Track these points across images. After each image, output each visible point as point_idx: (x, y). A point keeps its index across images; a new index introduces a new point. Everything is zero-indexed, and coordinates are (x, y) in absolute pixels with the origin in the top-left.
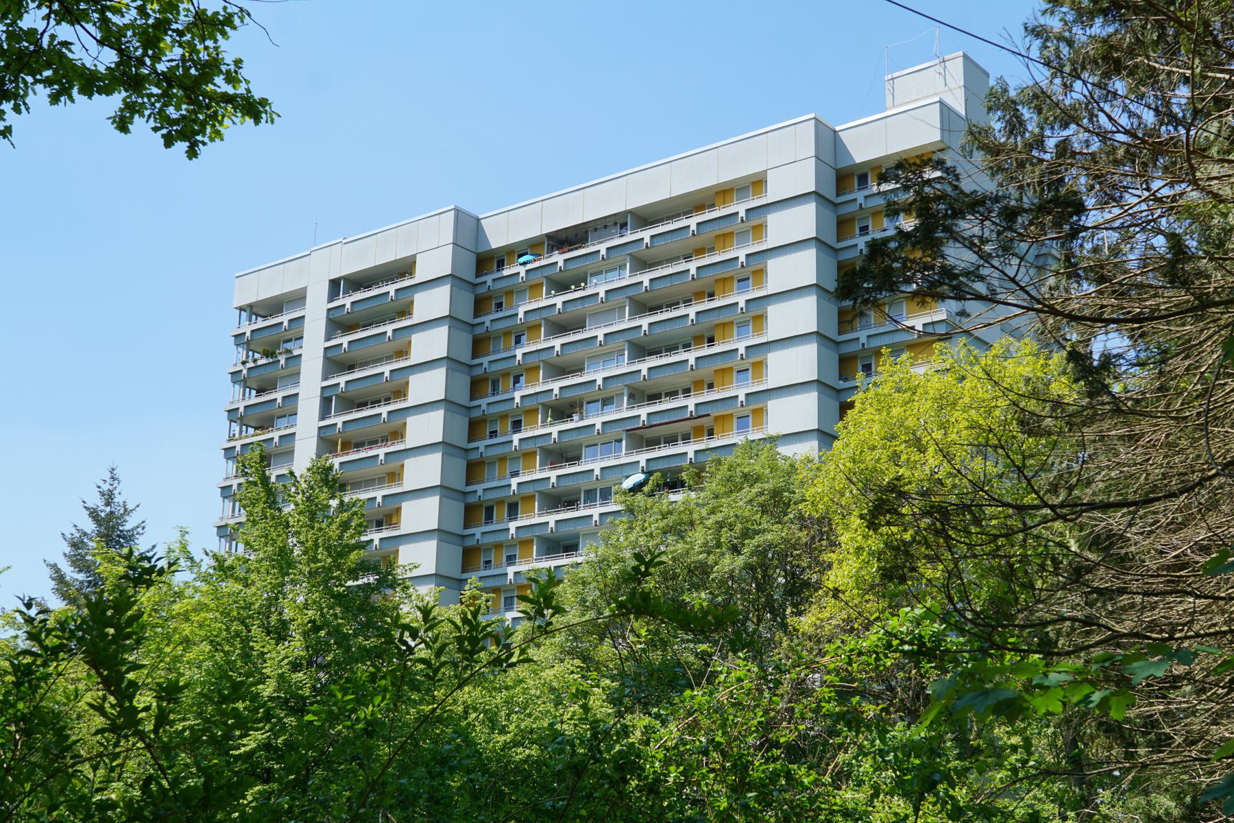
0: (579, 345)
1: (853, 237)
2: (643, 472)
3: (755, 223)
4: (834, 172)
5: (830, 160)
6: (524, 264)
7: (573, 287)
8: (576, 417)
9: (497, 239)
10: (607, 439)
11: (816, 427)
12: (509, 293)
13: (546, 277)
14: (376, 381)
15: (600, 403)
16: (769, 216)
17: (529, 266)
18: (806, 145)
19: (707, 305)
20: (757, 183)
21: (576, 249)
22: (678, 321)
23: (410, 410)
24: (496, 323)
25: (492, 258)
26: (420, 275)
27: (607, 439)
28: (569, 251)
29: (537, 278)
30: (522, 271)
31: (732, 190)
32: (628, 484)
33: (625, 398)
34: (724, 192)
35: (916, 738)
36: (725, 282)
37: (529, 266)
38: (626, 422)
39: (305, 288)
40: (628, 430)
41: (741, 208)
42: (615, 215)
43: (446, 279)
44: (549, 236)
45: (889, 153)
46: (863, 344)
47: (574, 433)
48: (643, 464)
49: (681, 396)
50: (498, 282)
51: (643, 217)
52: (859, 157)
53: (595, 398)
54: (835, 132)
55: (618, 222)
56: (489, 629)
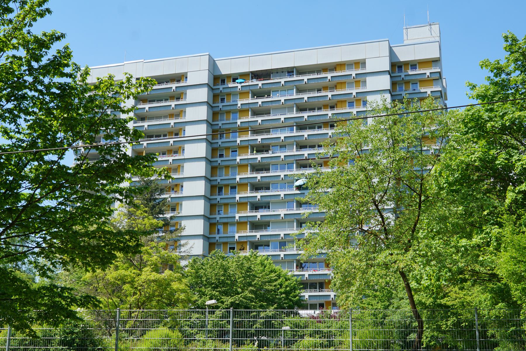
0: (270, 121)
1: (218, 103)
3: (360, 80)
4: (213, 76)
5: (212, 72)
6: (241, 83)
7: (266, 96)
8: (270, 152)
9: (225, 69)
11: (204, 175)
12: (229, 94)
13: (251, 90)
14: (166, 127)
15: (279, 147)
17: (243, 84)
18: (205, 65)
20: (361, 63)
21: (267, 80)
22: (322, 116)
23: (186, 142)
24: (225, 107)
25: (219, 78)
27: (286, 164)
28: (264, 80)
29: (246, 90)
30: (239, 86)
31: (345, 64)
33: (295, 146)
34: (341, 65)
35: (513, 292)
36: (343, 102)
37: (243, 84)
38: (296, 157)
39: (187, 73)
41: (353, 73)
42: (288, 68)
44: (252, 73)
45: (232, 72)
46: (220, 145)
49: (316, 148)
50: (225, 89)
51: (301, 71)
52: (224, 72)
54: (214, 60)
55: (290, 71)
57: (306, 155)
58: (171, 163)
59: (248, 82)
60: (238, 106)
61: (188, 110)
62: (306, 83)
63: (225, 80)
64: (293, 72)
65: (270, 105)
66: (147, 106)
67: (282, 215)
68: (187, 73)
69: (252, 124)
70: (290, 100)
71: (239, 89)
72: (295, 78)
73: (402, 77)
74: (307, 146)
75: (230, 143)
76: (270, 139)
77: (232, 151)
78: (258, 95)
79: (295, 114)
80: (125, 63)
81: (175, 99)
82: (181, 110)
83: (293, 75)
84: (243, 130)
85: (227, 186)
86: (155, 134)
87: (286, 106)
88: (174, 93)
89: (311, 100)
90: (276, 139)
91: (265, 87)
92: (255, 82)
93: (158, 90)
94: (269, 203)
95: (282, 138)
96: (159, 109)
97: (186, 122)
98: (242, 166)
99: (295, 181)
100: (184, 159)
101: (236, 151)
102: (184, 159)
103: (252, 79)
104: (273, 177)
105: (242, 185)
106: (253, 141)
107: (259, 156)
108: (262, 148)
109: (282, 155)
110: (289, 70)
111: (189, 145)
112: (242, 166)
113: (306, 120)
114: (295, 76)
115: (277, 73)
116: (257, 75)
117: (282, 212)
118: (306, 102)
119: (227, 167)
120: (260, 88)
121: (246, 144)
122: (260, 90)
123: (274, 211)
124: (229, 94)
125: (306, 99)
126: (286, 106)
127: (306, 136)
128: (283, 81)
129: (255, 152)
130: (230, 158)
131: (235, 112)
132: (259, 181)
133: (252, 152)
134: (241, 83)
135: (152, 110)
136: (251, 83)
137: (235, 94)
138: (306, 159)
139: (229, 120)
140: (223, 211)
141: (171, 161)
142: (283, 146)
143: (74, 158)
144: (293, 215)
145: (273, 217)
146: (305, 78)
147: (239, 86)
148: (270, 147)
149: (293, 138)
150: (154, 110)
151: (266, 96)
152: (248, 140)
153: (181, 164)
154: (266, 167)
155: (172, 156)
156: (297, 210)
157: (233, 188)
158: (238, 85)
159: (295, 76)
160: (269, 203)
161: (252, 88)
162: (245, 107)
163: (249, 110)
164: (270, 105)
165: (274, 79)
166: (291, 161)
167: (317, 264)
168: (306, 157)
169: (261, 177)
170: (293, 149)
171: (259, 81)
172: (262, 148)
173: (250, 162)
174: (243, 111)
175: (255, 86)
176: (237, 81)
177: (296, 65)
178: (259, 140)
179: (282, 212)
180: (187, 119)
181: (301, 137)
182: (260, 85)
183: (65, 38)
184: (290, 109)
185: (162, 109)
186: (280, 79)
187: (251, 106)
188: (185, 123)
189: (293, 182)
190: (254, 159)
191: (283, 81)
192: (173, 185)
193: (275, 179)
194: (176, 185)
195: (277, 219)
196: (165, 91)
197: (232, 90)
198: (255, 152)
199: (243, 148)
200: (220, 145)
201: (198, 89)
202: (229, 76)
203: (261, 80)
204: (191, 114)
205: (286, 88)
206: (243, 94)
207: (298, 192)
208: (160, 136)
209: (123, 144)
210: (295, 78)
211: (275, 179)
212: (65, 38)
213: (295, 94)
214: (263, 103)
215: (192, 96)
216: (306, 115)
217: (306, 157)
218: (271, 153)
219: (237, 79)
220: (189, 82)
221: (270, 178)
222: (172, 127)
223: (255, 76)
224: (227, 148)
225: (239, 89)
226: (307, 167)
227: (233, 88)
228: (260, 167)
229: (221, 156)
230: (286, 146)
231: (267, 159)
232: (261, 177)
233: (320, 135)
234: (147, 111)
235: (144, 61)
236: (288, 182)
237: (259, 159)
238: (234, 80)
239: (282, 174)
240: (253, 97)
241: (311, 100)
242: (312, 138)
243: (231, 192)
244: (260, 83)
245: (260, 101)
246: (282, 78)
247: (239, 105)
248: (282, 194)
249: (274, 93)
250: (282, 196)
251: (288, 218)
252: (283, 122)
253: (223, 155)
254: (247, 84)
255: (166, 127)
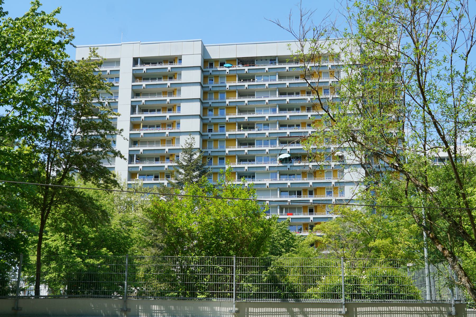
2: (288, 153)
6: (229, 67)
8: (256, 129)
10: (270, 140)
12: (217, 77)
14: (162, 103)
15: (263, 125)
16: (181, 104)
17: (231, 69)
19: (252, 115)
26: (184, 63)
27: (270, 140)
30: (228, 70)
32: (283, 156)
37: (231, 69)
39: (120, 58)
40: (279, 137)
43: (198, 67)
44: (239, 59)
45: (221, 57)
47: (255, 135)
48: (288, 150)
51: (282, 60)
53: (261, 123)
55: (272, 60)
56: (360, 107)
57: (288, 133)
58: (167, 135)
59: (235, 67)
60: (227, 87)
61: (183, 89)
62: (287, 71)
63: (213, 63)
64: (275, 60)
65: (255, 88)
66: (144, 84)
67: (268, 185)
68: (181, 56)
69: (239, 104)
70: (274, 85)
71: (228, 73)
72: (277, 66)
73: (210, 88)
74: (148, 110)
75: (220, 119)
76: (256, 118)
77: (220, 127)
78: (244, 79)
79: (277, 97)
80: (122, 43)
81: (168, 78)
82: (176, 88)
83: (276, 63)
84: (230, 108)
85: (216, 157)
86: (149, 109)
87: (270, 90)
88: (169, 73)
89: (292, 86)
90: (261, 118)
91: (251, 72)
92: (241, 67)
93: (154, 70)
94: (254, 173)
95: (267, 117)
96: (155, 87)
97: (181, 99)
98: (230, 141)
99: (278, 155)
100: (180, 132)
101: (224, 127)
102: (180, 132)
103: (238, 64)
104: (259, 151)
105: (231, 157)
106: (240, 119)
107: (246, 133)
108: (249, 126)
109: (267, 132)
110: (273, 59)
111: (184, 120)
112: (230, 141)
113: (288, 103)
114: (277, 64)
115: (262, 60)
116: (243, 61)
117: (267, 182)
118: (288, 87)
119: (216, 140)
120: (246, 72)
121: (234, 121)
122: (247, 74)
123: (260, 181)
124: (217, 77)
125: (288, 84)
126: (270, 90)
127: (288, 117)
128: (267, 68)
129: (242, 128)
130: (219, 133)
131: (222, 92)
132: (246, 154)
133: (239, 128)
134: (229, 67)
135: (148, 87)
136: (238, 68)
137: (222, 77)
138: (288, 137)
139: (217, 99)
140: (212, 179)
141: (167, 133)
142: (266, 125)
143: (84, 58)
144: (277, 185)
145: (259, 185)
146: (287, 66)
147: (228, 70)
148: (254, 124)
149: (276, 118)
150: (151, 87)
151: (252, 80)
152: (236, 118)
153: (177, 137)
154: (252, 142)
155: (168, 129)
156: (280, 180)
157: (222, 159)
158: (226, 69)
159: (277, 64)
160: (254, 173)
161: (238, 72)
162: (232, 89)
163: (236, 91)
164: (255, 88)
165: (259, 66)
166: (275, 137)
167: (297, 226)
168: (288, 135)
169: (248, 150)
170: (276, 127)
171: (246, 66)
172: (249, 126)
173: (238, 137)
174: (231, 92)
175: (242, 71)
176: (225, 65)
177: (278, 55)
178: (246, 118)
179: (267, 182)
180: (183, 96)
181: (283, 117)
182: (246, 70)
183: (60, 13)
184: (273, 92)
185: (158, 87)
186: (265, 65)
187: (238, 88)
188: (180, 101)
189: (276, 156)
190: (242, 135)
191: (267, 68)
192: (169, 155)
193: (259, 153)
194: (172, 155)
195: (263, 187)
196: (161, 71)
197: (221, 73)
198: (242, 128)
199: (230, 124)
200: (210, 121)
201: (192, 71)
202: (216, 61)
203: (247, 66)
204: (186, 93)
205: (268, 74)
206: (230, 77)
207: (281, 165)
208: (293, 126)
209: (368, 204)
210: (277, 66)
211: (259, 153)
212: (60, 13)
213: (277, 80)
214: (249, 86)
215: (186, 76)
216: (288, 98)
217: (288, 135)
218: (257, 130)
219: (224, 63)
220: (184, 64)
221: (256, 151)
222: (168, 103)
223: (241, 61)
224: (216, 124)
225: (228, 73)
226: (286, 143)
227: (222, 72)
228: (243, 142)
229: (210, 130)
230: (268, 124)
231: (253, 135)
232: (248, 150)
233: (301, 117)
234: (144, 88)
235: (141, 43)
236: (272, 156)
237: (246, 135)
238: (222, 64)
239: (267, 149)
240: (239, 80)
241: (292, 86)
242: (293, 119)
243: (219, 163)
244: (246, 69)
245: (246, 84)
246: (266, 65)
247: (228, 87)
248: (267, 166)
249: (257, 77)
250: (267, 167)
251: (273, 187)
252: (267, 104)
253: (212, 130)
254: (235, 68)
255: (162, 103)
